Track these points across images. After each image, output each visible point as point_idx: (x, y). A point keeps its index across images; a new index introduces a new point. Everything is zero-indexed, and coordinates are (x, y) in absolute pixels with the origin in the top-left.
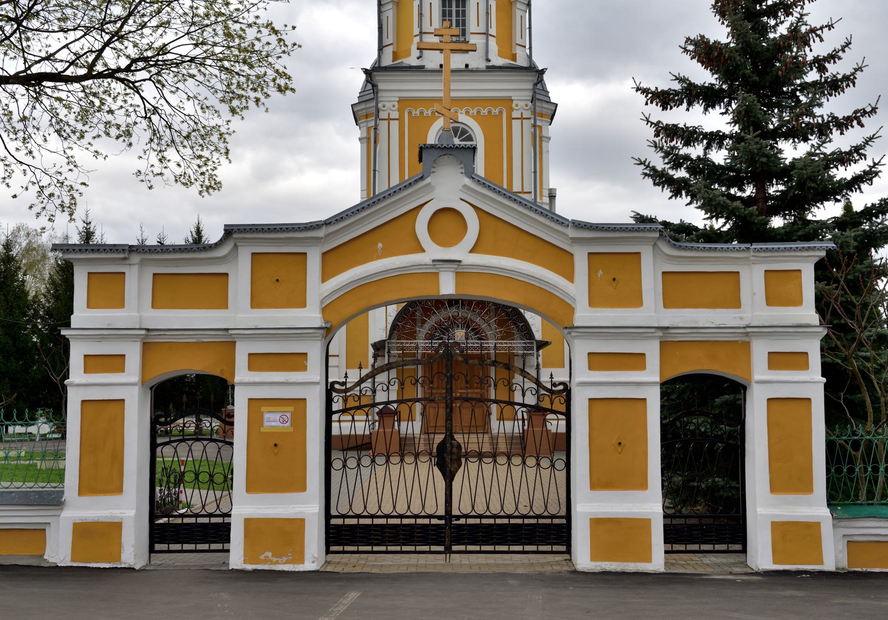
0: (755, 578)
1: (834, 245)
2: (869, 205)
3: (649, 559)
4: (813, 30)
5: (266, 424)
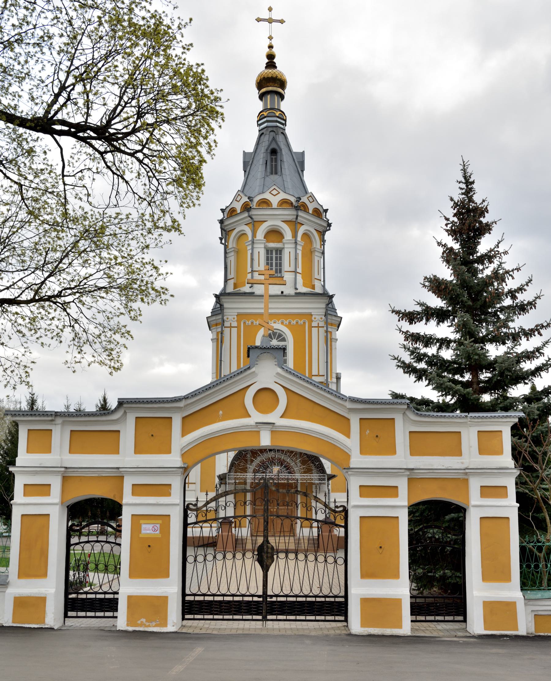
0: (472, 640)
1: (524, 414)
2: (546, 387)
3: (400, 627)
4: (507, 272)
5: (143, 532)
